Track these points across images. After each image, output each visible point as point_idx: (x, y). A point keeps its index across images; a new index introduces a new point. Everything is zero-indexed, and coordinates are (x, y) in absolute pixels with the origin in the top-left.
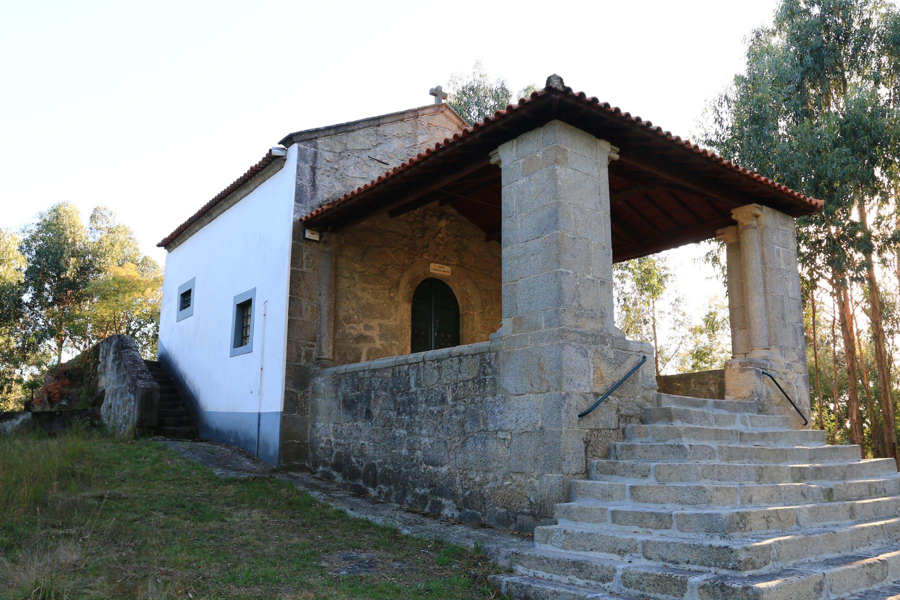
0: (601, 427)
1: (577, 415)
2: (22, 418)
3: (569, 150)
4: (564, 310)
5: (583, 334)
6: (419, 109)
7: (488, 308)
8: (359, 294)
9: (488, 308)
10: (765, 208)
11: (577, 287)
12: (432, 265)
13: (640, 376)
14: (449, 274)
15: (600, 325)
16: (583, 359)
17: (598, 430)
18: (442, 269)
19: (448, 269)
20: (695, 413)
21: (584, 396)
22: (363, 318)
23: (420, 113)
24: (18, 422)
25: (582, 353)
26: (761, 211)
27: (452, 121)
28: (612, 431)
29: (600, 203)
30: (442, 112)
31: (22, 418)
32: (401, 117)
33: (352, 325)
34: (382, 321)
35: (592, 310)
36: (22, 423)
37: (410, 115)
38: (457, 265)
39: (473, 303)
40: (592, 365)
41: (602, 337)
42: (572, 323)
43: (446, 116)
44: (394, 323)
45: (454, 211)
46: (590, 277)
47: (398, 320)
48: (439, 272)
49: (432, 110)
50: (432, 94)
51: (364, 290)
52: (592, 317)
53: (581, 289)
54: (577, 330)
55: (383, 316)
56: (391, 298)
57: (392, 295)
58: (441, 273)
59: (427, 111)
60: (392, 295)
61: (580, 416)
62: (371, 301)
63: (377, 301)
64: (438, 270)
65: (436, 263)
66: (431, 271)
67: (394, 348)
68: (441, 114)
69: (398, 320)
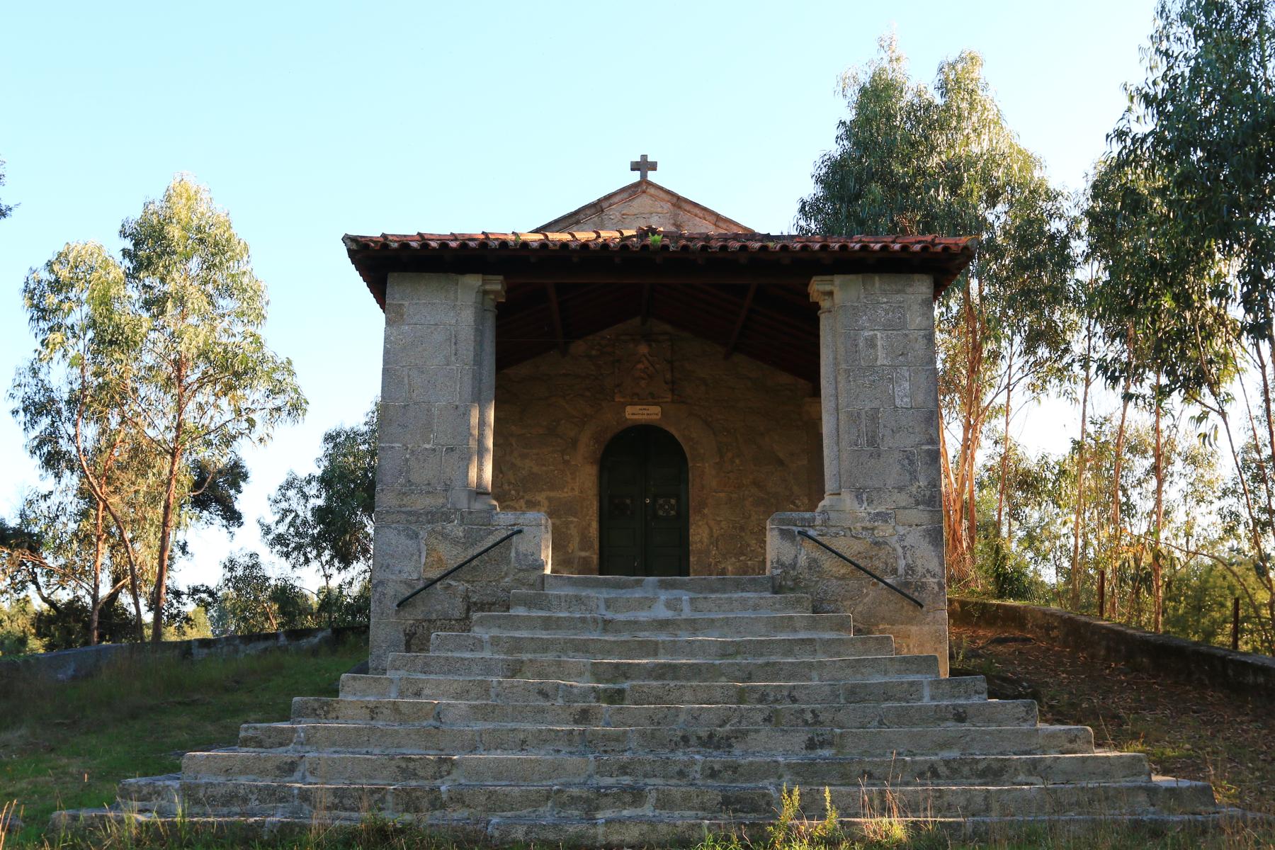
0: (434, 616)
1: (395, 605)
2: (320, 635)
3: (406, 303)
4: (382, 490)
5: (410, 513)
6: (600, 201)
7: (730, 455)
8: (518, 462)
9: (730, 455)
10: (838, 279)
11: (407, 460)
12: (629, 409)
13: (513, 554)
14: (658, 417)
15: (441, 501)
16: (409, 542)
17: (430, 621)
18: (645, 412)
19: (657, 409)
20: (559, 597)
21: (408, 584)
22: (525, 492)
23: (605, 205)
24: (316, 640)
25: (408, 535)
26: (832, 284)
27: (663, 200)
28: (453, 622)
29: (456, 354)
30: (644, 192)
31: (320, 635)
32: (574, 219)
33: (508, 503)
34: (552, 494)
35: (429, 484)
36: (320, 642)
37: (588, 212)
38: (673, 402)
39: (702, 451)
40: (424, 548)
41: (443, 513)
42: (395, 502)
43: (652, 196)
44: (570, 494)
45: (668, 328)
46: (427, 446)
47: (576, 489)
48: (640, 417)
49: (625, 195)
50: (632, 169)
51: (524, 456)
52: (428, 492)
53: (412, 463)
54: (403, 509)
55: (552, 487)
56: (566, 463)
57: (567, 457)
58: (645, 417)
59: (616, 199)
60: (567, 457)
61: (398, 605)
62: (536, 469)
63: (544, 468)
64: (638, 413)
65: (636, 404)
66: (628, 417)
67: (572, 526)
68: (644, 195)
69: (576, 489)
